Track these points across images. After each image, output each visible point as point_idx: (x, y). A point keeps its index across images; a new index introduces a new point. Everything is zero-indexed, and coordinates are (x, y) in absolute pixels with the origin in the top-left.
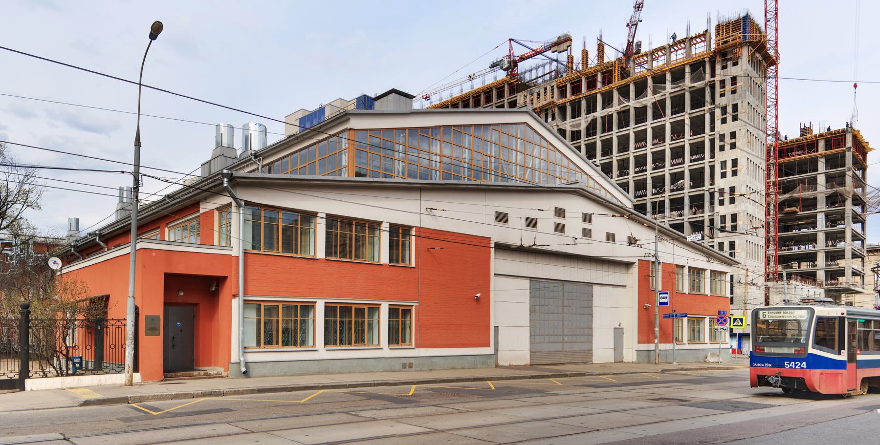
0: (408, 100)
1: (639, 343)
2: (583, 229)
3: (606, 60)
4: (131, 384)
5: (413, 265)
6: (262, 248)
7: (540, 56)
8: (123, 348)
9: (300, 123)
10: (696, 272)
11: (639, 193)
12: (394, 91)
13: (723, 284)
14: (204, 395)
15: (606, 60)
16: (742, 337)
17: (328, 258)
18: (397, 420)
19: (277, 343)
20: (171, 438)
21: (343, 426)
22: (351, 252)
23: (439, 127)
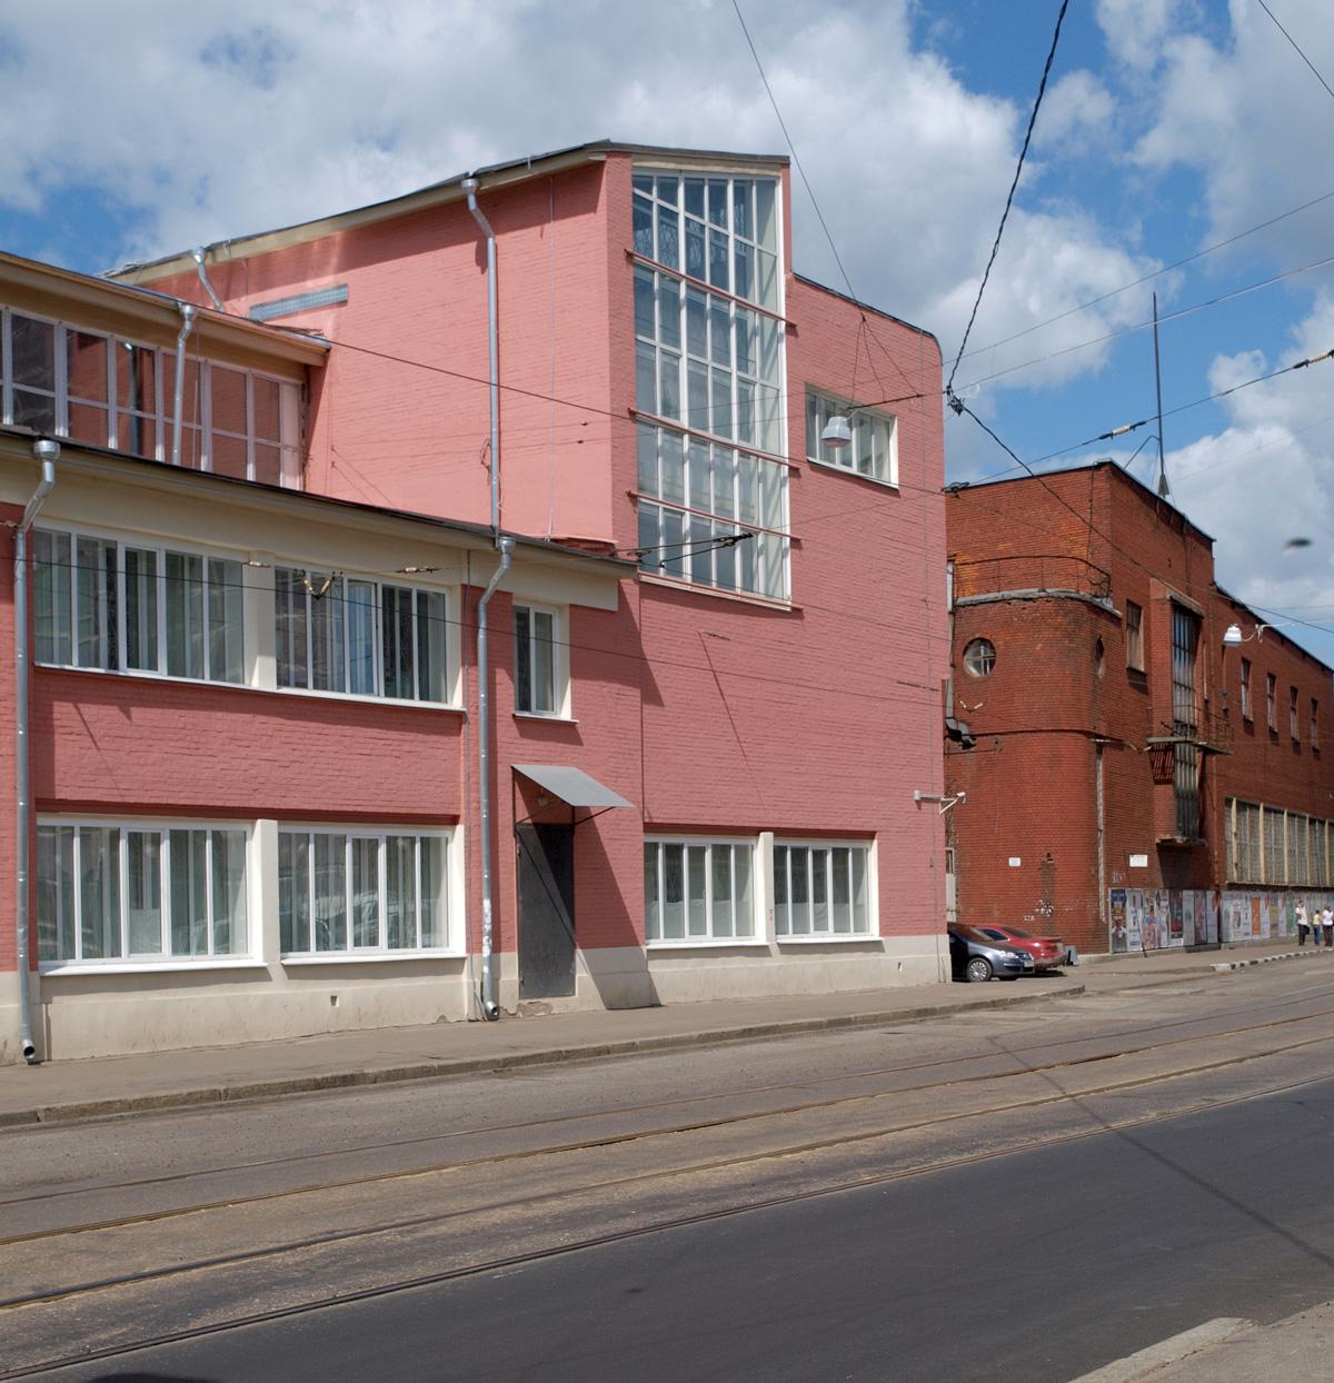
5: (894, 481)
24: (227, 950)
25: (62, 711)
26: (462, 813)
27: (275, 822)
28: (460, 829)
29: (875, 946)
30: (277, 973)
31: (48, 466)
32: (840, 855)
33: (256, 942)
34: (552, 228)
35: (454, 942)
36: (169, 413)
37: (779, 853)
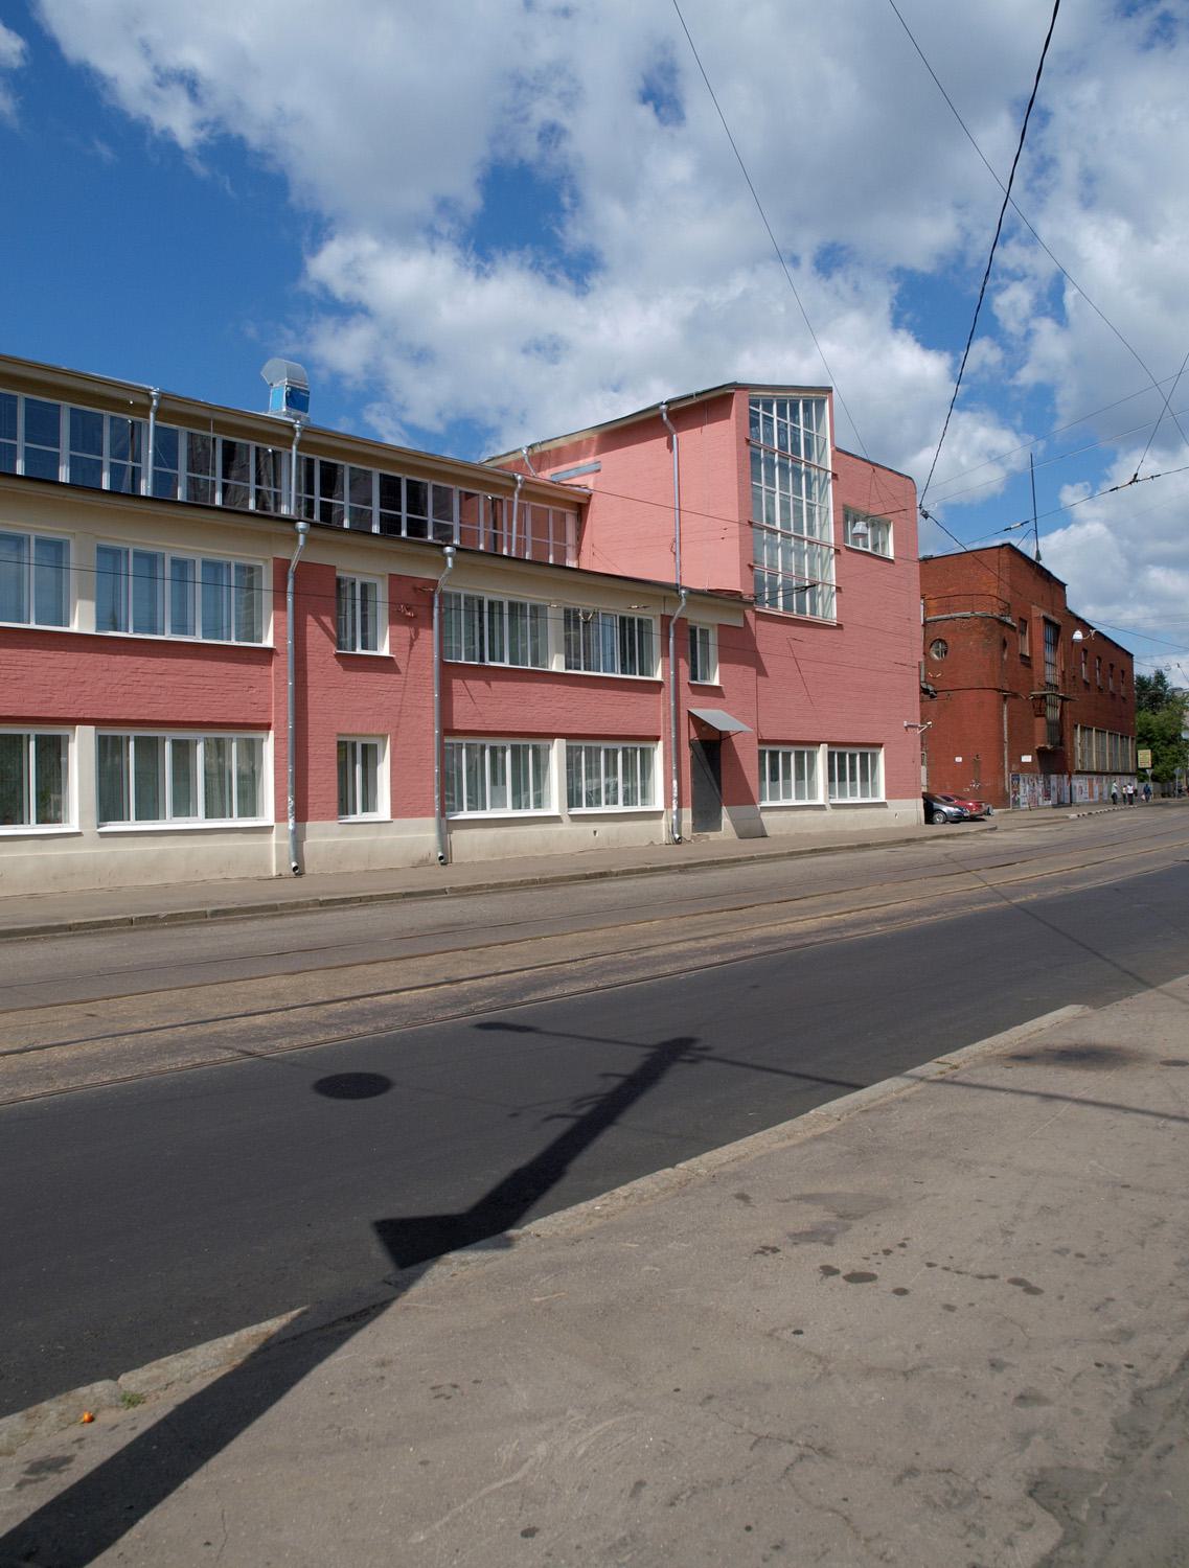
0: (254, 670)
1: (197, 815)
2: (363, 811)
3: (666, 438)
4: (881, 1558)
5: (891, 555)
6: (529, 663)
7: (968, 549)
8: (101, 430)
9: (408, 621)
10: (432, 676)
11: (789, 592)
12: (910, 478)
13: (608, 629)
14: (793, 948)
15: (666, 438)
16: (766, 1413)
17: (576, 811)
18: (502, 517)
19: (231, 816)
20: (70, 378)
21: (32, 916)
22: (127, 625)
23: (146, 917)
24: (540, 807)
25: (457, 684)
26: (662, 734)
27: (564, 740)
28: (661, 743)
29: (883, 805)
30: (566, 819)
31: (683, 600)
32: (800, 755)
33: (555, 804)
34: (706, 428)
35: (658, 803)
36: (510, 530)
37: (831, 755)
